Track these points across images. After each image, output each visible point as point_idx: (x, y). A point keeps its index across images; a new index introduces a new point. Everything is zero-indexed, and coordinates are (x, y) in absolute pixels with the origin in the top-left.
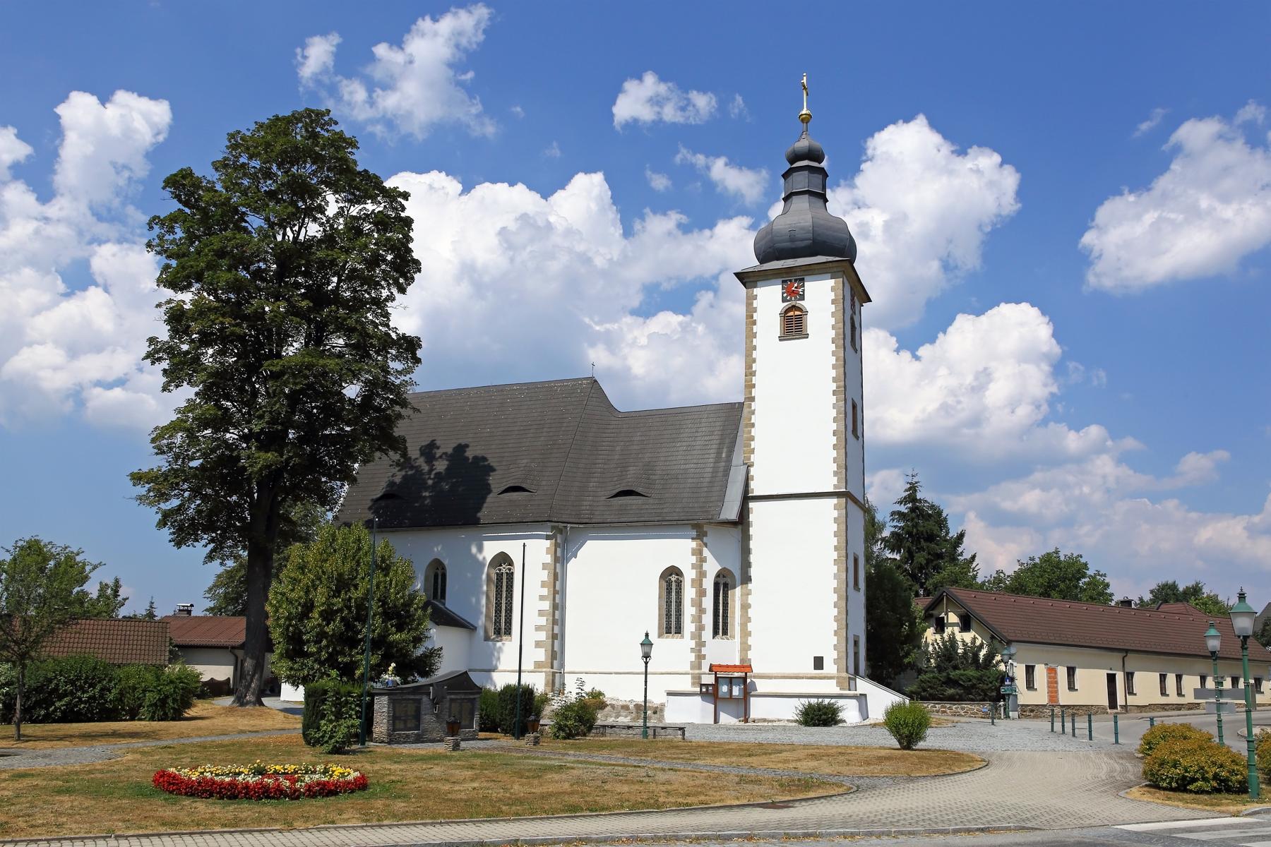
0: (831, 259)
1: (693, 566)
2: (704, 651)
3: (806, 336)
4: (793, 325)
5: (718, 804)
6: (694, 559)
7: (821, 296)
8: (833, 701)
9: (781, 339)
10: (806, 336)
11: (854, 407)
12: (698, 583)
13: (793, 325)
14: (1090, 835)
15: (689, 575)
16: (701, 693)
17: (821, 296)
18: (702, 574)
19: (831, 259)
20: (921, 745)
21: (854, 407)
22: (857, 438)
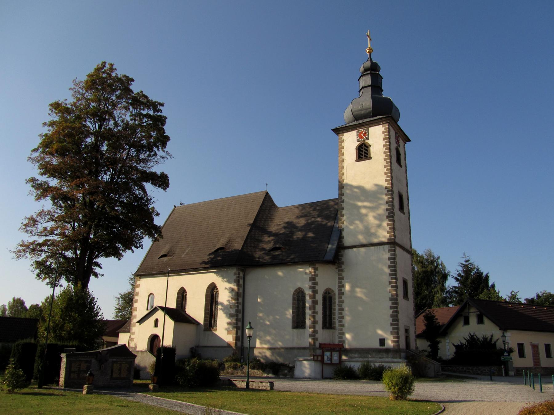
0: (381, 117)
1: (311, 287)
2: (317, 336)
3: (371, 158)
4: (363, 152)
5: (440, 411)
6: (310, 283)
7: (377, 135)
8: (383, 364)
9: (357, 161)
10: (371, 158)
11: (398, 161)
12: (313, 297)
13: (363, 152)
14: (168, 391)
15: (308, 292)
16: (314, 360)
17: (377, 135)
18: (315, 292)
19: (381, 117)
20: (409, 397)
21: (398, 161)
22: (401, 166)
